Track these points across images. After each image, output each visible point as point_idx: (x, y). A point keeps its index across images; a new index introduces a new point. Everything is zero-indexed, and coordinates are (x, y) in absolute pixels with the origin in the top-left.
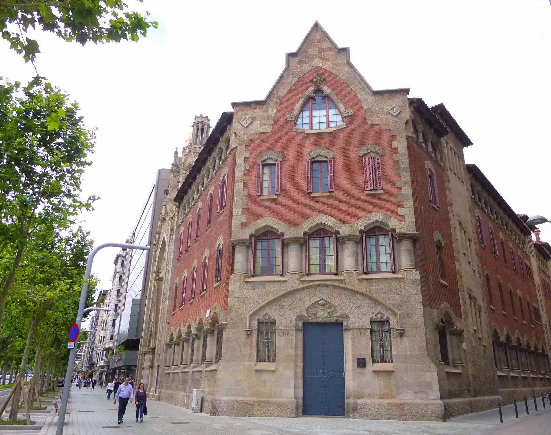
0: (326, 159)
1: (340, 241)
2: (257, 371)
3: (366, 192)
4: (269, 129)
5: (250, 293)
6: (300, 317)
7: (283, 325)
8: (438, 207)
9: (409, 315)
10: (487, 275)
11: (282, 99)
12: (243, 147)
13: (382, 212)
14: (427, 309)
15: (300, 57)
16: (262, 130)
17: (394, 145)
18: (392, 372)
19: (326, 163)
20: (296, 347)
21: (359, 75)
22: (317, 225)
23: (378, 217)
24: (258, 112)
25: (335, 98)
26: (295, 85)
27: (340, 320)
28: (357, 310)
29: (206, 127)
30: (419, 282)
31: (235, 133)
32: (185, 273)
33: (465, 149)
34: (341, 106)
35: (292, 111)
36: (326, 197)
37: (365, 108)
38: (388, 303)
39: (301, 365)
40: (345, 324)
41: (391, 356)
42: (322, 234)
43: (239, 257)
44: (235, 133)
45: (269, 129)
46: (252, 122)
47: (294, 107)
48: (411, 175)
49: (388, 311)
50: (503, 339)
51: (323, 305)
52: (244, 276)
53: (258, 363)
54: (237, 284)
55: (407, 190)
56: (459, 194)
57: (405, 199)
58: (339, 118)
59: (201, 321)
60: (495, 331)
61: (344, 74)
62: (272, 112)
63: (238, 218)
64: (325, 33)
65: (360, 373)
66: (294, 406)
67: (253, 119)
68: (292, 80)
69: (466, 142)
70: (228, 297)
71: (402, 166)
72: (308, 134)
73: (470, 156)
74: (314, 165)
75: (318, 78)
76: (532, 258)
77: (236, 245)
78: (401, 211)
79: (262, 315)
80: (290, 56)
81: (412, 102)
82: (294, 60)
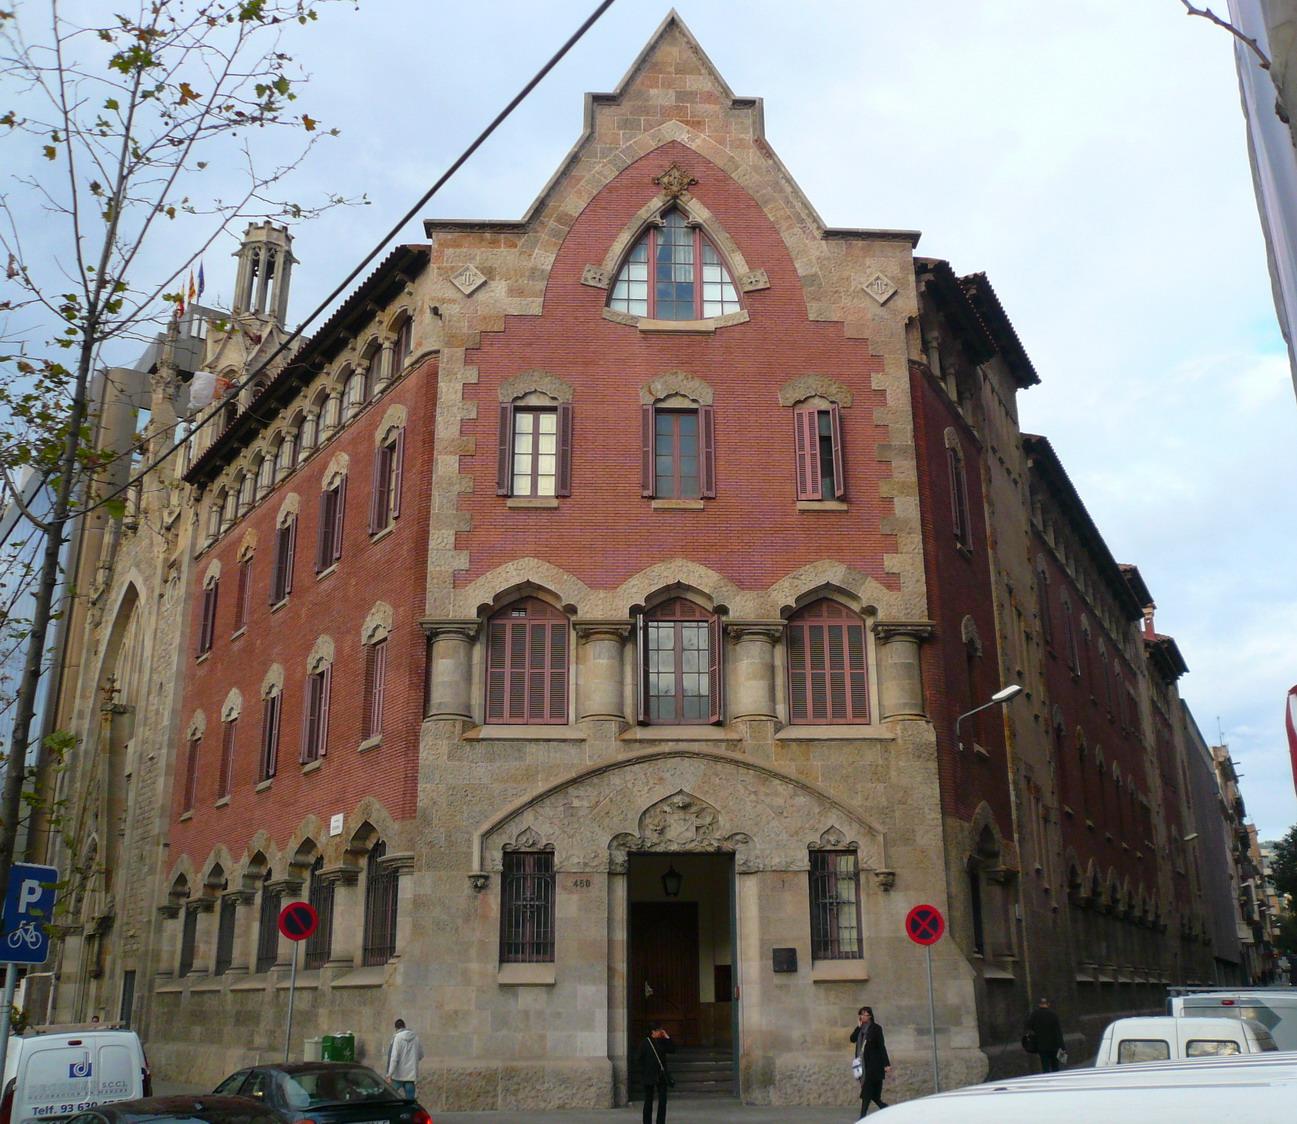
0: (694, 406)
1: (729, 635)
2: (503, 986)
3: (801, 505)
4: (535, 307)
5: (479, 770)
6: (620, 839)
7: (576, 860)
8: (970, 552)
9: (907, 838)
10: (1059, 725)
11: (571, 223)
12: (460, 352)
13: (842, 561)
14: (950, 821)
15: (626, 105)
16: (514, 306)
17: (877, 381)
18: (864, 981)
19: (692, 418)
20: (610, 920)
21: (789, 180)
22: (668, 588)
23: (832, 573)
24: (504, 255)
25: (722, 238)
26: (609, 188)
27: (728, 846)
28: (775, 823)
29: (280, 259)
30: (933, 750)
31: (435, 311)
32: (234, 703)
33: (1020, 393)
34: (738, 261)
35: (599, 262)
36: (693, 510)
37: (801, 272)
38: (856, 802)
39: (622, 966)
40: (739, 858)
41: (860, 941)
42: (678, 613)
43: (445, 666)
44: (435, 311)
45: (535, 307)
46: (484, 284)
47: (606, 250)
48: (918, 468)
49: (855, 826)
50: (1084, 893)
51: (685, 807)
52: (464, 721)
53: (505, 965)
54: (444, 746)
55: (907, 507)
56: (1008, 511)
57: (901, 530)
58: (730, 293)
59: (308, 845)
60: (1073, 867)
61: (745, 170)
62: (544, 258)
63: (443, 555)
64: (696, 50)
65: (780, 987)
66: (608, 1078)
67: (490, 273)
68: (600, 172)
69: (1025, 375)
70: (415, 780)
71: (895, 443)
72: (642, 332)
73: (1033, 411)
74: (663, 418)
75: (677, 174)
76: (1140, 677)
77: (437, 634)
78: (891, 562)
79: (515, 833)
80: (598, 100)
81: (921, 266)
82: (607, 116)
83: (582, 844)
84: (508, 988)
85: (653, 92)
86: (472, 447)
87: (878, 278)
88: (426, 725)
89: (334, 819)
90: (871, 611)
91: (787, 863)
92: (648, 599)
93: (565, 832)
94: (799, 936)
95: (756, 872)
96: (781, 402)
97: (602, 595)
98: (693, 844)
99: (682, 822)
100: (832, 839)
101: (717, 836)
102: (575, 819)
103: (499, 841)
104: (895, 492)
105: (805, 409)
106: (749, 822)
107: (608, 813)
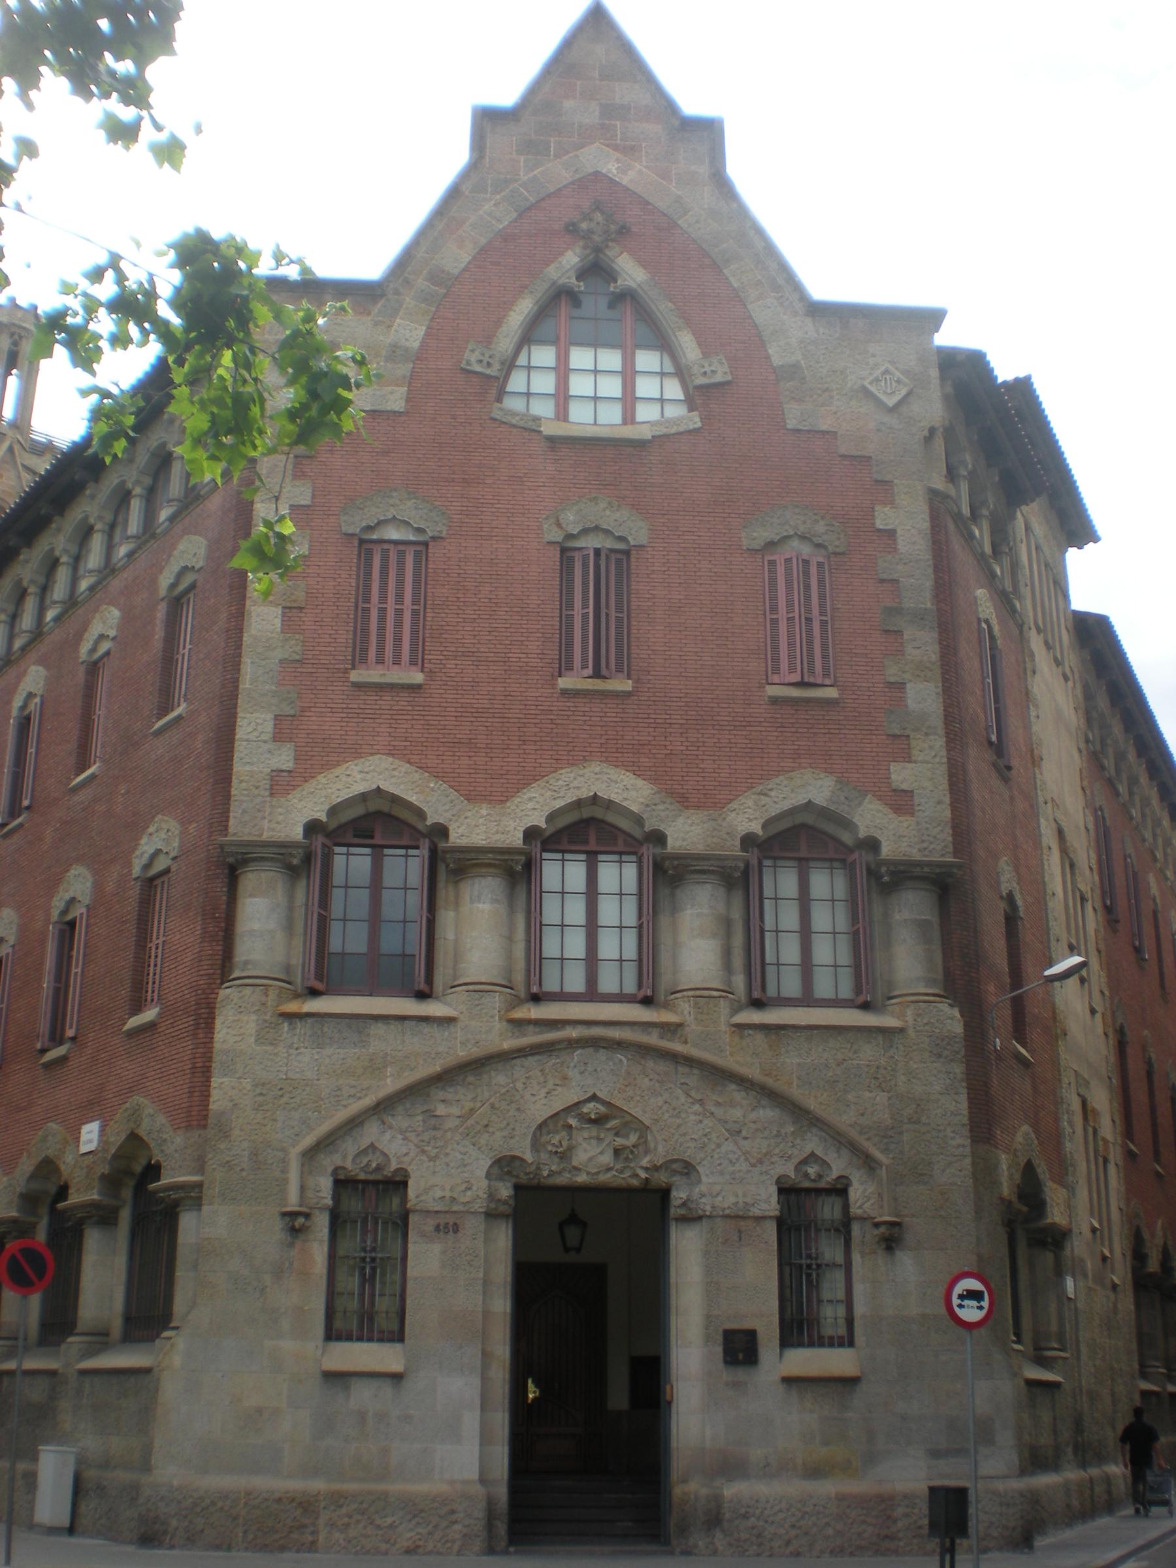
3: (772, 691)
6: (505, 1165)
7: (439, 1194)
13: (829, 771)
17: (884, 517)
23: (814, 788)
25: (663, 309)
27: (662, 1178)
28: (728, 1146)
34: (688, 345)
35: (488, 340)
38: (844, 1120)
41: (850, 1321)
47: (498, 323)
54: (251, 1024)
63: (257, 751)
66: (479, 1512)
68: (493, 213)
83: (450, 1170)
84: (336, 1378)
85: (568, 104)
86: (301, 595)
87: (886, 372)
88: (223, 993)
89: (86, 1128)
90: (872, 845)
91: (746, 1204)
92: (550, 818)
93: (423, 1152)
94: (762, 1311)
95: (700, 1218)
96: (745, 543)
97: (484, 812)
98: (609, 1175)
99: (594, 1142)
100: (812, 1171)
101: (645, 1162)
102: (438, 1134)
103: (330, 1161)
104: (907, 676)
105: (779, 557)
106: (692, 1144)
107: (487, 1126)
